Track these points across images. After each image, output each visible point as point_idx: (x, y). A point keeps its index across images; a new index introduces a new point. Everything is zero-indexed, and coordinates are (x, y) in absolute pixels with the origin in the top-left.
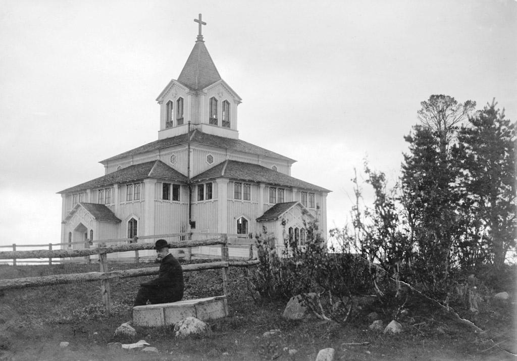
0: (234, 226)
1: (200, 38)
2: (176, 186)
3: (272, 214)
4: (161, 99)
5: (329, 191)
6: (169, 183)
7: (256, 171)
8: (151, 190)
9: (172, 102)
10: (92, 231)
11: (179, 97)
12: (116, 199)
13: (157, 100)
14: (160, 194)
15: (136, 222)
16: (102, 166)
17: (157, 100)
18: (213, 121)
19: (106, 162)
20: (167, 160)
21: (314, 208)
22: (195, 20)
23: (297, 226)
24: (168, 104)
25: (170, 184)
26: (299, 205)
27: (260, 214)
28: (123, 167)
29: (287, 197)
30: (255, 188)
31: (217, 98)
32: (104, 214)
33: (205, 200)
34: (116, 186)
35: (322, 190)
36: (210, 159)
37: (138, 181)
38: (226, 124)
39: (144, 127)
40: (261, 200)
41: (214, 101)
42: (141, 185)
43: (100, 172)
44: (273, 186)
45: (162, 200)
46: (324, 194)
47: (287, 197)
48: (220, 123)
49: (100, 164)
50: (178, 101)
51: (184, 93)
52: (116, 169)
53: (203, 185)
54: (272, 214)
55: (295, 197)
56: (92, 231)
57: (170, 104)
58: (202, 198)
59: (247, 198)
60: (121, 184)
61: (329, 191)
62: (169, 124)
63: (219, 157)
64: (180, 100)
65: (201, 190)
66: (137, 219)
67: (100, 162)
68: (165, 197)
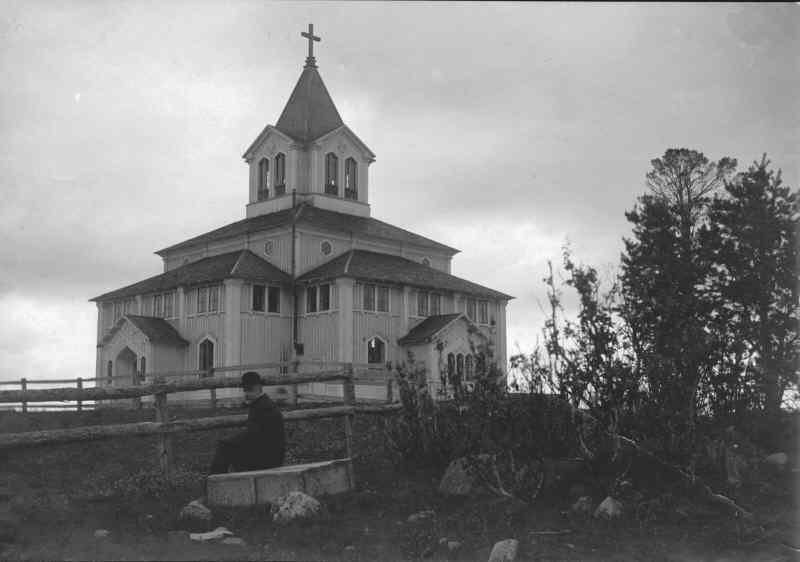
1: (311, 62)
2: (275, 289)
4: (250, 155)
5: (510, 298)
8: (234, 297)
9: (267, 160)
11: (261, 157)
12: (182, 310)
16: (160, 259)
18: (331, 190)
19: (165, 254)
20: (258, 249)
22: (304, 34)
24: (261, 164)
25: (264, 287)
31: (337, 153)
36: (326, 249)
37: (216, 282)
40: (406, 311)
41: (331, 159)
45: (363, 311)
47: (445, 307)
48: (341, 192)
50: (277, 158)
51: (285, 146)
52: (180, 264)
55: (457, 307)
56: (144, 358)
57: (264, 163)
59: (383, 307)
61: (510, 298)
64: (280, 157)
68: (258, 306)
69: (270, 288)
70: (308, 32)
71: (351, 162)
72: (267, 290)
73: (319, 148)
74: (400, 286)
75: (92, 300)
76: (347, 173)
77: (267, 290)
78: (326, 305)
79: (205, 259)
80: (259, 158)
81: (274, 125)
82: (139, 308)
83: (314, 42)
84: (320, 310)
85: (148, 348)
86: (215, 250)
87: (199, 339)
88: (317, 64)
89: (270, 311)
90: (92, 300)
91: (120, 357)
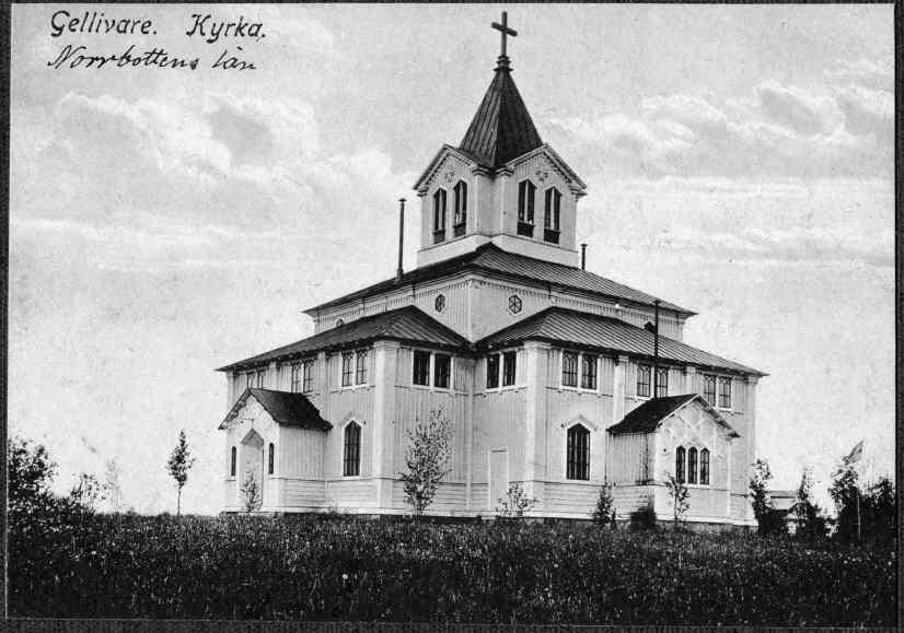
0: (13, 299)
1: (504, 67)
2: (436, 352)
3: (644, 420)
4: (422, 186)
5: (760, 375)
6: (429, 350)
7: (623, 331)
8: (385, 364)
9: (444, 193)
10: (272, 445)
11: (437, 189)
12: (326, 383)
13: (416, 188)
14: (409, 374)
15: (358, 429)
16: (309, 319)
17: (416, 188)
18: (525, 230)
19: (317, 312)
20: (425, 304)
21: (576, 386)
22: (495, 26)
23: (694, 444)
24: (436, 196)
25: (429, 354)
26: (699, 400)
27: (617, 419)
28: (348, 320)
29: (675, 385)
30: (678, 374)
31: (535, 181)
32: (297, 412)
33: (500, 388)
34: (322, 356)
35: (747, 370)
36: (516, 304)
37: (364, 346)
38: (552, 237)
39: (377, 244)
40: (621, 388)
41: (527, 190)
42: (369, 353)
43: (301, 329)
44: (654, 364)
45: (412, 385)
46: (751, 379)
47: (675, 385)
48: (539, 231)
49: (306, 315)
50: (457, 188)
51: (466, 172)
52: (332, 325)
53: (498, 356)
54: (644, 420)
55: (691, 384)
56: (272, 445)
57: (440, 195)
58: (493, 382)
59: (590, 382)
60: (330, 352)
61: (760, 375)
62: (439, 235)
63: (534, 303)
64: (461, 187)
65: (493, 368)
66: (359, 423)
67: (307, 312)
68: (420, 376)
69: (436, 355)
70: (500, 22)
71: (554, 197)
72: (432, 359)
73: (510, 173)
74: (614, 356)
75: (222, 370)
76: (457, 211)
77: (432, 359)
78: (510, 379)
79: (362, 319)
80: (433, 190)
81: (457, 143)
82: (280, 381)
83: (509, 36)
84: (504, 385)
85: (276, 428)
86: (378, 306)
87: (587, 422)
88: (511, 66)
89: (436, 385)
90: (222, 370)
91: (244, 442)
